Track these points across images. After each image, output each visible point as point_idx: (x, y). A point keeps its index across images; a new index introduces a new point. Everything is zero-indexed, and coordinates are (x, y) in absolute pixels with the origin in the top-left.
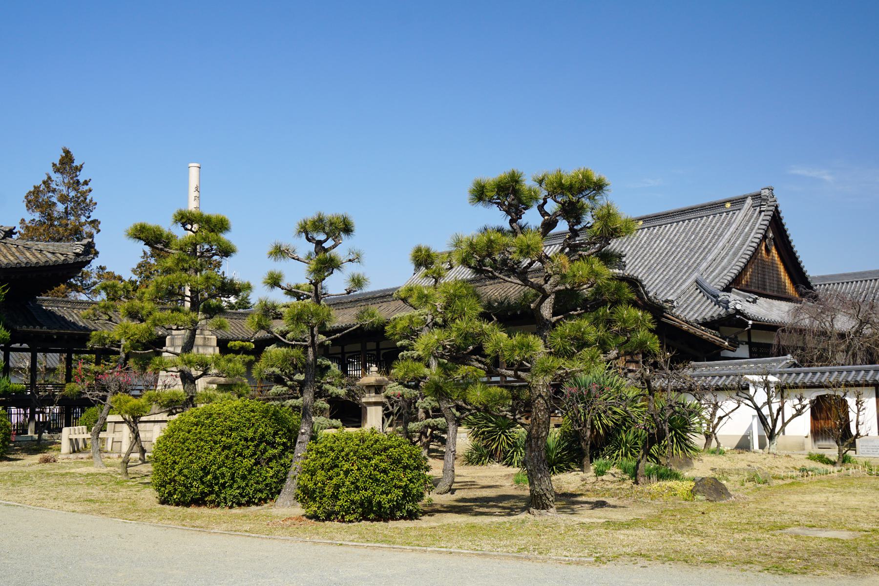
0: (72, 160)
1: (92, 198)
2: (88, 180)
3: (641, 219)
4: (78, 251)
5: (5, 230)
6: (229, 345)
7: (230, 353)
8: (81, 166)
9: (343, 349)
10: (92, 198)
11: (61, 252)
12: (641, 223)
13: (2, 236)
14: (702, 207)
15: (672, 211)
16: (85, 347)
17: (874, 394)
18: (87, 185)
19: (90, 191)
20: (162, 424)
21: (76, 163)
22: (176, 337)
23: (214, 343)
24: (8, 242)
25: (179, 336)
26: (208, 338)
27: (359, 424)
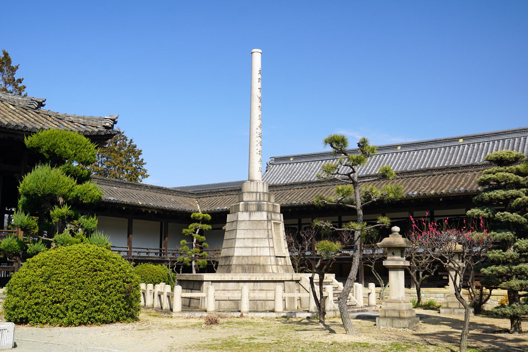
0: (9, 61)
1: (27, 93)
2: (21, 78)
3: (462, 138)
4: (107, 124)
5: (38, 101)
6: (192, 216)
7: (195, 222)
8: (17, 67)
9: (300, 221)
10: (27, 93)
11: (91, 125)
12: (461, 140)
13: (36, 106)
14: (513, 131)
15: (488, 133)
16: (443, 199)
17: (400, 254)
18: (21, 83)
19: (25, 87)
20: (262, 284)
21: (13, 64)
22: (249, 203)
23: (279, 210)
24: (41, 112)
25: (253, 203)
26: (275, 205)
27: (346, 278)
